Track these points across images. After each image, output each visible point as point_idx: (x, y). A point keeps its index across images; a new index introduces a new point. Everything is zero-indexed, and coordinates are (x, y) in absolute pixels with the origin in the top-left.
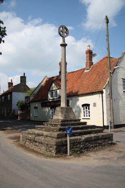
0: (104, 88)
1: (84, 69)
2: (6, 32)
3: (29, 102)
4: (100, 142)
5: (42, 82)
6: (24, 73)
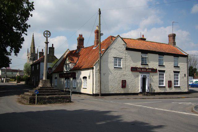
0: (94, 65)
1: (93, 47)
2: (34, 7)
3: (51, 73)
4: (60, 100)
5: (64, 55)
6: (53, 45)
